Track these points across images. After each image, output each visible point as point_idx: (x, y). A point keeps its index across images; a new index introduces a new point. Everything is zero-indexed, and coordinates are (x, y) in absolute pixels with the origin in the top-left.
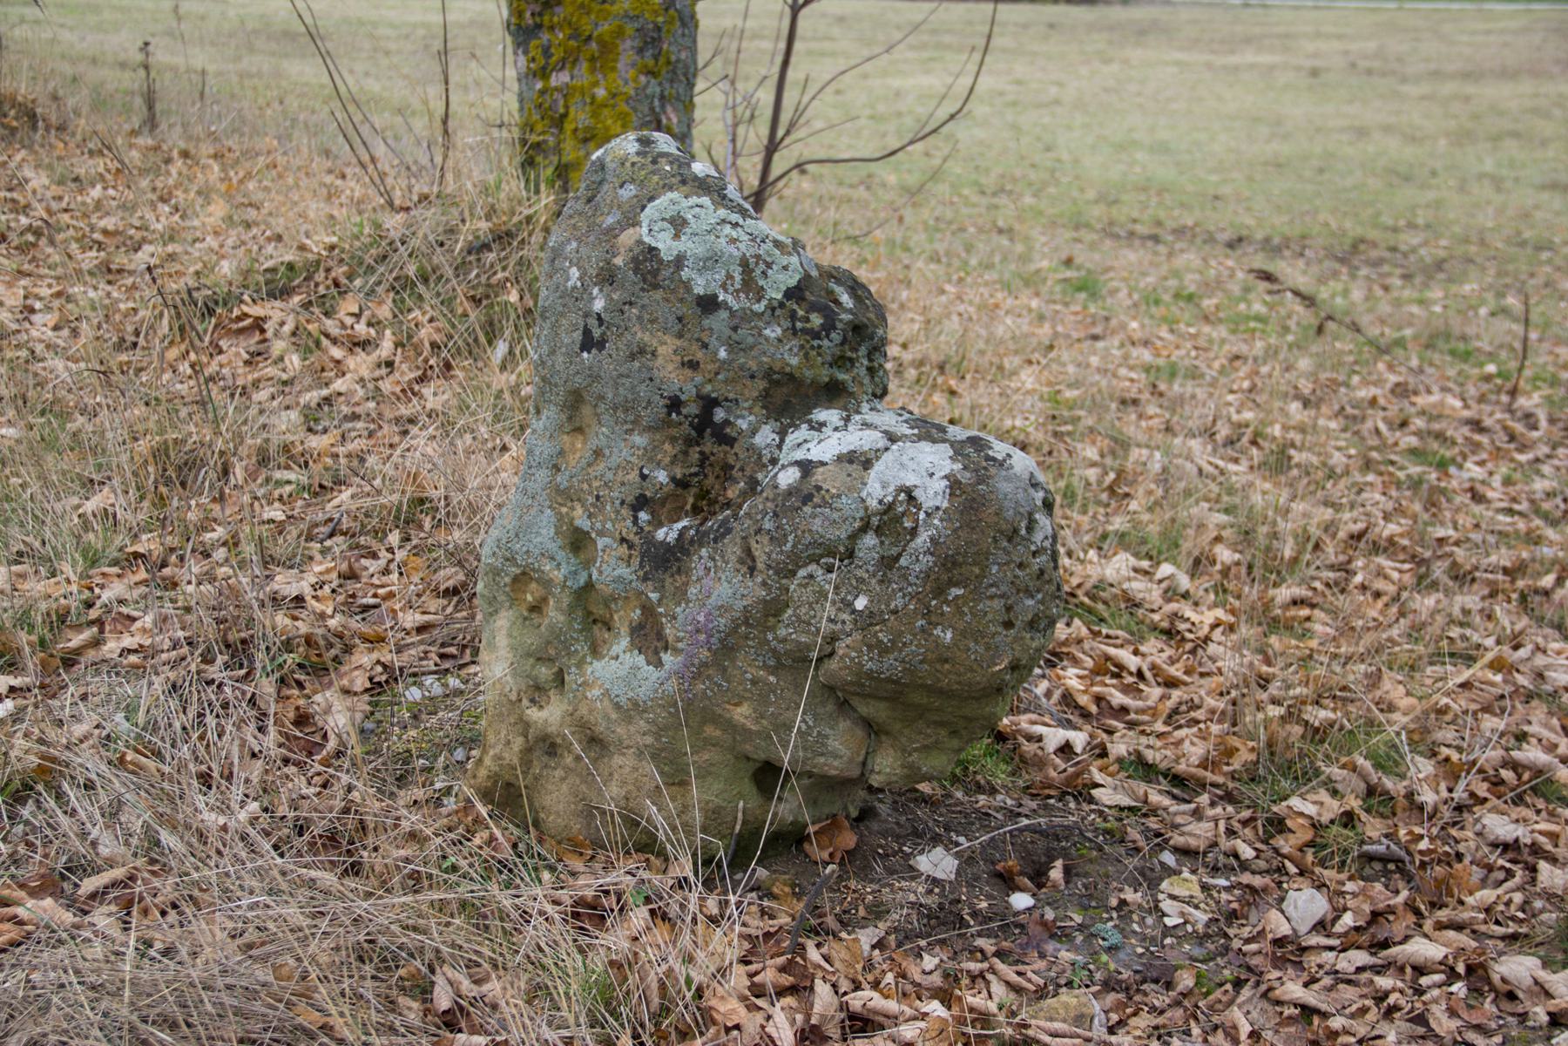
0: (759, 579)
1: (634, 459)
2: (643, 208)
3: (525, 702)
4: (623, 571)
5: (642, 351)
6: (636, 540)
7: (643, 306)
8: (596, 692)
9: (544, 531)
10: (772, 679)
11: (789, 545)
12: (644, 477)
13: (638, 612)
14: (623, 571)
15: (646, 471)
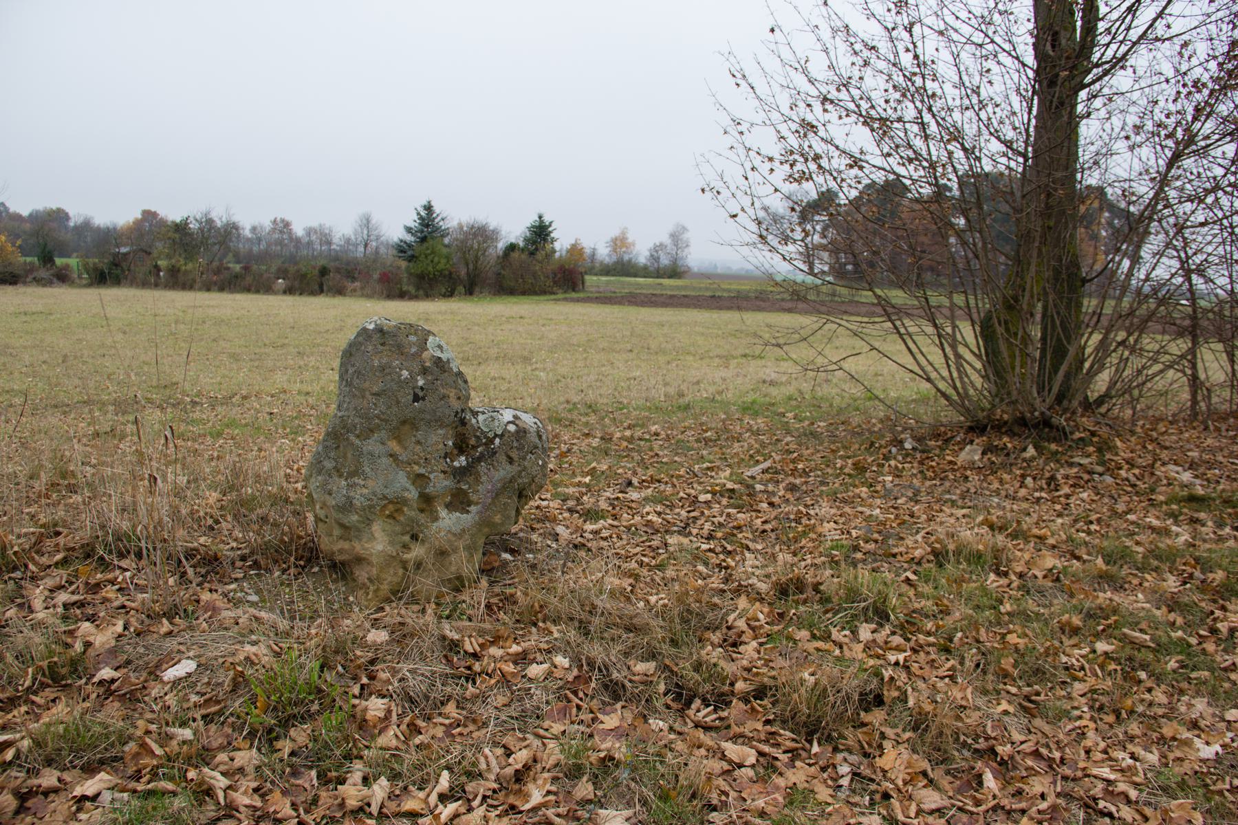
4: (447, 483)
8: (442, 534)
14: (447, 483)
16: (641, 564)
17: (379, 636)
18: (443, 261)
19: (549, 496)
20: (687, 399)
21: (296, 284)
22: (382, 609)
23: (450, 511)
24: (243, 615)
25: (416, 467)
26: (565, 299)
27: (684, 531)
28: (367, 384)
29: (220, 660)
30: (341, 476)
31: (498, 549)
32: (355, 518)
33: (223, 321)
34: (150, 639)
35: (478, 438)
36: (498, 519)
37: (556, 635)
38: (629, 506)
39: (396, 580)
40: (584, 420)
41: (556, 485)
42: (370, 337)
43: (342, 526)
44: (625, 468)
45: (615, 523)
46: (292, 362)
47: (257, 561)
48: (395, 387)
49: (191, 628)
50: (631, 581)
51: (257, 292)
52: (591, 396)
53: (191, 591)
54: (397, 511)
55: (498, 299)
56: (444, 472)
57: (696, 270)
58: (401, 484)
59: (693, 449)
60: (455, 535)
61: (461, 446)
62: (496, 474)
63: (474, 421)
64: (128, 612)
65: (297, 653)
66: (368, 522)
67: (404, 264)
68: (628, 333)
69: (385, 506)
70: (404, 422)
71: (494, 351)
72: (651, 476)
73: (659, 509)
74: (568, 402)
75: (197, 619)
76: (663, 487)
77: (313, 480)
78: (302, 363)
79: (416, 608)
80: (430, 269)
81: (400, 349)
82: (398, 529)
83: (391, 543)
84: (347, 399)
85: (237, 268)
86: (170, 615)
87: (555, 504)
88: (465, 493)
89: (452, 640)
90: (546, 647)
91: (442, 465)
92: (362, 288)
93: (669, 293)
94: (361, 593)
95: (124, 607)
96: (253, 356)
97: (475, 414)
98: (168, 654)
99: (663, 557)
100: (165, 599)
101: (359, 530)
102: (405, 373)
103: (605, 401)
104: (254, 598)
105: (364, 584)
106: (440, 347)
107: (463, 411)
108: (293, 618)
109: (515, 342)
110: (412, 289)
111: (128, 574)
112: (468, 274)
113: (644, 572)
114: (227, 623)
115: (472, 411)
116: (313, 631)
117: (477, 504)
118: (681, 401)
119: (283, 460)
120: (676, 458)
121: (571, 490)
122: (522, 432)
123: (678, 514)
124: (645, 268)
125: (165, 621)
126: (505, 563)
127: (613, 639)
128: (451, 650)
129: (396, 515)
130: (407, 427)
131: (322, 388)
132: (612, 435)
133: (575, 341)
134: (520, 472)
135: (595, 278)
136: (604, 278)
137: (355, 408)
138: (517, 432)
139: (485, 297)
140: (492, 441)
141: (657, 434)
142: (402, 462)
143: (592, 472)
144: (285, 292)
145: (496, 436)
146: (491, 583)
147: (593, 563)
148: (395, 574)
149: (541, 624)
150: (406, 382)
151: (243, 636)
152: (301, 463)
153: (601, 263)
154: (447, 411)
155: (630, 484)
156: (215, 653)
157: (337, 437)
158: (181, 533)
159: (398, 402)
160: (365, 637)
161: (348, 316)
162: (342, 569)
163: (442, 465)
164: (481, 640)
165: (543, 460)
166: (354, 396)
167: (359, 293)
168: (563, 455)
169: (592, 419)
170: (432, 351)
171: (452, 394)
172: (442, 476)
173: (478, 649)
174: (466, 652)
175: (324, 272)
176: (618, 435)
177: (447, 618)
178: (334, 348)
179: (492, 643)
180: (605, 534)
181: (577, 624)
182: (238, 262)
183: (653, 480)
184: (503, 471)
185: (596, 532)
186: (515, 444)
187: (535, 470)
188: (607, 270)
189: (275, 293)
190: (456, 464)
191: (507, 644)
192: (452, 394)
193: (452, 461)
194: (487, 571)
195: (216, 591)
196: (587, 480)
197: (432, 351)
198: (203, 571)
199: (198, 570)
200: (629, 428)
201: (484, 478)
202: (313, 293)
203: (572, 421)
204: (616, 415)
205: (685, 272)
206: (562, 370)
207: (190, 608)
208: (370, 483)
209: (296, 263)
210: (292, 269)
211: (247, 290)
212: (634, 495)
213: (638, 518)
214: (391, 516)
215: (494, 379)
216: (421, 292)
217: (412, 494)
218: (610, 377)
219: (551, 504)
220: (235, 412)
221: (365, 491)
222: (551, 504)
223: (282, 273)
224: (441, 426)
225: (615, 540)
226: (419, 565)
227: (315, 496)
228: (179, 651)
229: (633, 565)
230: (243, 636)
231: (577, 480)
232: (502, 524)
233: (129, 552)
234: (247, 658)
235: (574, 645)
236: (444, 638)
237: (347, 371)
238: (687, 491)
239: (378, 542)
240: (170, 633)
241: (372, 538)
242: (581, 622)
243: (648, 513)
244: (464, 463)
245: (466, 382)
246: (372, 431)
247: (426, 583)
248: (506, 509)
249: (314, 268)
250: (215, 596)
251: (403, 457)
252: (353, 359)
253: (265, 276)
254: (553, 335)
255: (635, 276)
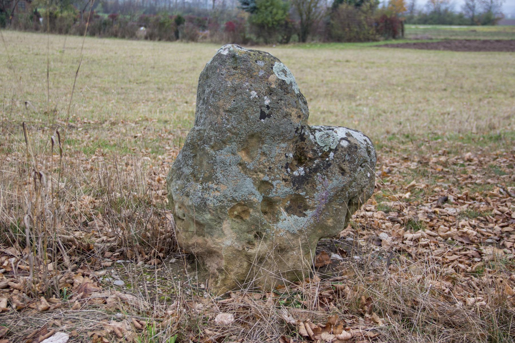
0: (348, 175)
1: (282, 152)
2: (272, 68)
3: (246, 249)
4: (287, 189)
5: (287, 115)
6: (289, 178)
7: (286, 100)
8: (282, 233)
9: (248, 186)
10: (340, 207)
11: (356, 162)
12: (287, 157)
13: (289, 202)
14: (287, 189)
15: (287, 155)
16: (457, 269)
17: (226, 318)
18: (281, 12)
19: (373, 208)
20: (498, 132)
21: (156, 31)
22: (228, 296)
23: (289, 214)
24: (111, 296)
25: (261, 175)
26: (386, 46)
27: (499, 243)
28: (221, 103)
29: (90, 334)
30: (197, 181)
31: (330, 250)
32: (208, 216)
33: (94, 61)
34: (30, 315)
35: (315, 151)
36: (330, 222)
37: (381, 325)
38: (446, 219)
39: (241, 271)
40: (402, 147)
41: (379, 199)
42: (224, 61)
43: (198, 223)
44: (441, 187)
45: (433, 233)
46: (152, 96)
47: (121, 252)
48: (245, 105)
49: (66, 306)
50: (448, 283)
51: (123, 37)
52: (408, 128)
53: (66, 275)
54: (244, 211)
55: (327, 45)
56: (285, 180)
57: (509, 16)
58: (248, 188)
59: (504, 173)
60: (294, 234)
61: (300, 159)
62: (330, 183)
63: (311, 137)
64: (11, 291)
65: (156, 329)
66: (219, 220)
67: (246, 15)
68: (443, 75)
69: (233, 208)
70: (252, 136)
71: (323, 90)
72: (466, 195)
73: (473, 222)
74: (388, 132)
75: (71, 298)
76: (477, 204)
77: (173, 184)
78: (161, 97)
79: (257, 296)
80: (269, 19)
81: (250, 72)
82: (244, 227)
83: (238, 239)
84: (203, 115)
85: (106, 16)
86: (48, 294)
87: (378, 215)
88: (302, 199)
89: (289, 324)
90: (372, 335)
91: (284, 174)
92: (212, 36)
93: (482, 38)
94: (211, 281)
95: (8, 287)
96: (120, 91)
97: (313, 131)
98: (45, 327)
99: (479, 264)
100: (44, 280)
101: (211, 227)
102: (254, 94)
103: (421, 132)
104: (121, 283)
105: (214, 274)
106: (284, 71)
107: (302, 127)
108: (152, 300)
109: (342, 82)
110: (253, 37)
111: (13, 260)
112: (302, 23)
113: (461, 276)
114: (97, 302)
115: (310, 128)
116: (170, 312)
117: (313, 208)
118: (492, 133)
119: (148, 171)
120: (489, 180)
121: (391, 204)
122: (353, 148)
123: (492, 228)
124: (461, 16)
125: (43, 299)
126: (336, 262)
127: (434, 333)
128: (288, 333)
129: (243, 215)
130: (254, 140)
131: (178, 117)
132: (429, 159)
133: (394, 81)
134: (351, 182)
135: (413, 27)
136: (422, 27)
137: (211, 123)
138: (350, 147)
139: (315, 44)
140: (327, 155)
141: (470, 160)
142: (250, 170)
143: (412, 189)
144: (146, 38)
145: (331, 150)
146: (323, 278)
147: (413, 267)
148: (241, 266)
149: (367, 315)
150: (255, 101)
151: (110, 313)
152: (161, 175)
153: (420, 13)
154: (289, 128)
155: (446, 200)
156: (85, 327)
157: (194, 147)
158: (60, 227)
159: (247, 119)
160: (213, 318)
161: (200, 59)
162: (194, 260)
163: (284, 174)
164: (314, 326)
165: (372, 173)
166: (210, 112)
167: (209, 39)
168: (384, 175)
169: (410, 146)
170: (277, 75)
171: (294, 112)
172: (283, 183)
173: (312, 333)
174: (301, 335)
175: (179, 21)
176: (434, 160)
177: (286, 305)
178: (188, 85)
179: (324, 329)
180: (423, 242)
181: (400, 317)
182: (106, 12)
183: (467, 197)
184: (335, 181)
185: (417, 240)
186: (347, 158)
187: (364, 181)
188: (425, 20)
189: (138, 38)
190: (296, 173)
191: (338, 331)
192: (294, 112)
193: (292, 171)
194: (320, 267)
195: (88, 276)
196: (407, 195)
197: (277, 75)
198: (77, 259)
199: (73, 258)
200: (444, 154)
201: (319, 187)
202: (169, 39)
203: (392, 148)
204: (432, 143)
205: (499, 19)
206: (383, 106)
207: (65, 289)
208: (222, 187)
209: (155, 14)
210: (152, 19)
211: (115, 35)
212: (451, 210)
213: (454, 230)
214: (238, 216)
215: (323, 112)
216: (261, 40)
217: (257, 198)
218: (426, 112)
219: (375, 215)
220: (105, 136)
221: (217, 194)
222: (375, 215)
223: (144, 22)
224: (284, 141)
225: (433, 248)
226: (261, 259)
227: (175, 197)
228: (54, 325)
229: (450, 270)
230: (110, 313)
231: (397, 196)
232: (334, 227)
233: (14, 242)
234: (113, 333)
235: (398, 335)
236: (282, 321)
237: (204, 91)
238: (501, 208)
239: (227, 238)
240: (46, 310)
241: (222, 234)
242: (404, 315)
243: (463, 226)
244: (303, 173)
245: (305, 103)
246: (224, 143)
247: (267, 274)
248: (337, 214)
249: (171, 17)
250: (87, 280)
251: (251, 166)
252: (209, 81)
253: (130, 24)
254: (375, 76)
255: (451, 24)
